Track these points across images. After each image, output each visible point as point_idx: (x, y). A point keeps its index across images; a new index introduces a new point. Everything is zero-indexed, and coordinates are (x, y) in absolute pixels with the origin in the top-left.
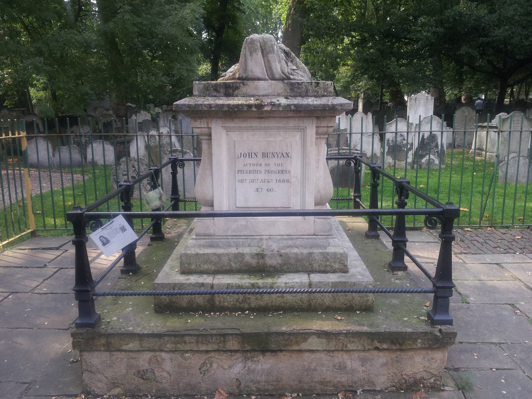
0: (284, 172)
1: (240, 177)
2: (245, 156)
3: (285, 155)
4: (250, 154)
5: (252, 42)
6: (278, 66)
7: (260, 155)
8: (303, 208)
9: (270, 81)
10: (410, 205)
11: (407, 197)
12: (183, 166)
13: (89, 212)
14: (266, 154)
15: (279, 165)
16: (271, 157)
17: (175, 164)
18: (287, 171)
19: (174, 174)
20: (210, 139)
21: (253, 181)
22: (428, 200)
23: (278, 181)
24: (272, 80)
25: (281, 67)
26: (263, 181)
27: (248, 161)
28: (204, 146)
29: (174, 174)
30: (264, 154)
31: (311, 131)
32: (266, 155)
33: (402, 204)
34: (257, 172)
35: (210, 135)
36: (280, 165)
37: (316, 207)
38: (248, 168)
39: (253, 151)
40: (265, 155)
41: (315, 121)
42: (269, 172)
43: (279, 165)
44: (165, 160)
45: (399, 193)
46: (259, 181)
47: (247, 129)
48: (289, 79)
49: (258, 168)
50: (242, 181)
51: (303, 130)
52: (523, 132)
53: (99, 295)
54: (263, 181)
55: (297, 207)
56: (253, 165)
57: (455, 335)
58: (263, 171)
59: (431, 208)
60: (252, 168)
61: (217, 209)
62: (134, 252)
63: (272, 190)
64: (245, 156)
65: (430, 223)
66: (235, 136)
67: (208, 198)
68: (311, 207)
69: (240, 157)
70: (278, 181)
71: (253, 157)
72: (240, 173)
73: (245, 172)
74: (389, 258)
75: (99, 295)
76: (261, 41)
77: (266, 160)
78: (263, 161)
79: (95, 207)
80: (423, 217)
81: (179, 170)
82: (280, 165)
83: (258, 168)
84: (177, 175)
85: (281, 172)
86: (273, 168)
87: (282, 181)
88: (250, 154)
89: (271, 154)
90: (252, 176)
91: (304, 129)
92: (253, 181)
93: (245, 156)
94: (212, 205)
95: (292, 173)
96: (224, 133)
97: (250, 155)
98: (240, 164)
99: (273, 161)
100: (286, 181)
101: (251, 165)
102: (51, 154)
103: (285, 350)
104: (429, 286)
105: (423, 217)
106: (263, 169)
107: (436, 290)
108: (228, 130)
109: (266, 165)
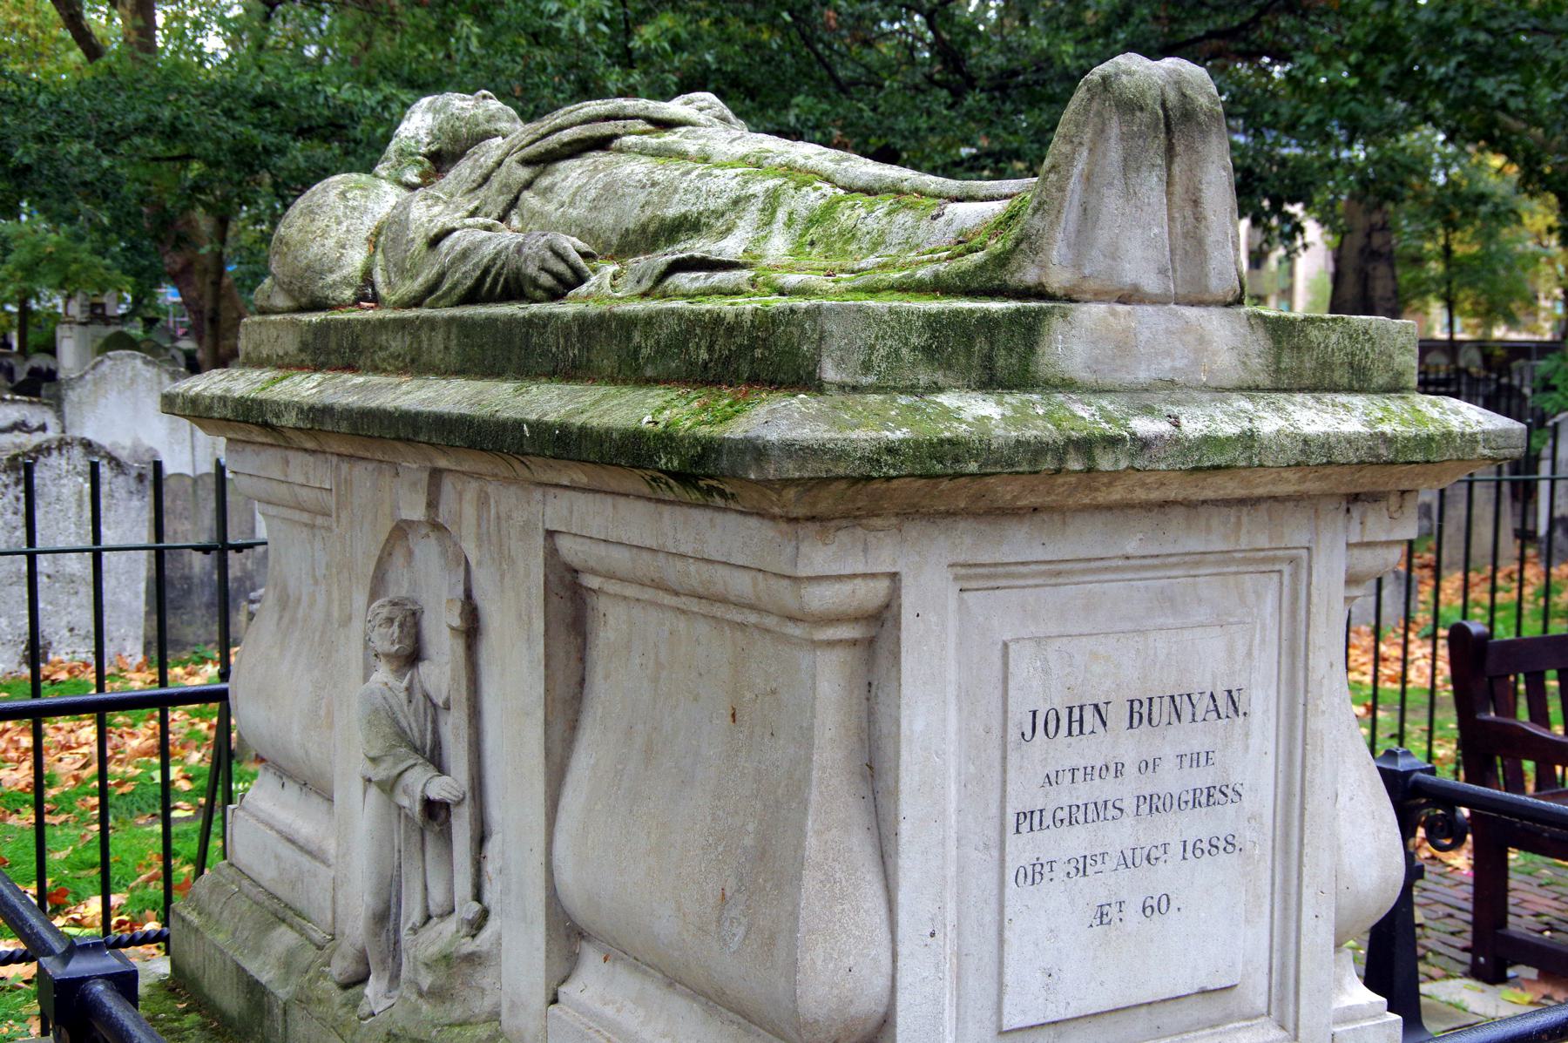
3: (1222, 701)
15: (1195, 760)
34: (1101, 810)
40: (1139, 713)
43: (1195, 760)
46: (1111, 863)
56: (1088, 772)
58: (1129, 804)
60: (1084, 792)
78: (1126, 745)
86: (1170, 780)
90: (1075, 841)
106: (1125, 790)
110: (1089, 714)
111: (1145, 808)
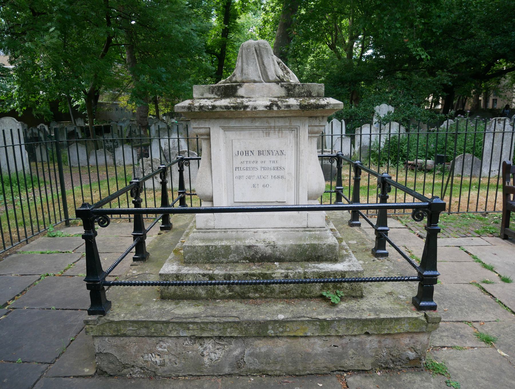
0: (279, 169)
1: (237, 173)
2: (242, 154)
4: (247, 152)
5: (248, 47)
6: (273, 69)
7: (256, 153)
8: (297, 203)
9: (265, 83)
10: (391, 199)
11: (389, 191)
12: (188, 164)
13: (98, 208)
14: (262, 152)
15: (274, 162)
16: (266, 154)
17: (182, 163)
18: (282, 168)
19: (181, 171)
20: (209, 139)
21: (250, 177)
22: (416, 196)
23: (273, 177)
24: (266, 82)
25: (276, 72)
26: (259, 177)
27: (245, 158)
28: (204, 145)
29: (181, 171)
30: (260, 152)
31: (304, 132)
32: (262, 152)
33: (384, 199)
35: (209, 135)
36: (275, 162)
37: (309, 201)
38: (245, 165)
39: (276, 171)
40: (260, 153)
41: (307, 121)
42: (264, 169)
43: (274, 162)
44: (174, 158)
45: (381, 186)
47: (243, 129)
48: (282, 81)
49: (254, 165)
50: (240, 177)
51: (297, 129)
52: (7, 147)
53: (110, 285)
54: (259, 177)
55: (291, 203)
57: (440, 319)
59: (418, 202)
60: (249, 165)
61: (217, 204)
62: (145, 242)
63: (267, 185)
64: (242, 153)
65: (418, 216)
66: (232, 135)
67: (208, 193)
68: (304, 202)
69: (237, 155)
70: (273, 177)
71: (249, 155)
72: (237, 170)
73: (242, 169)
74: (373, 245)
75: (110, 285)
76: (257, 46)
77: (262, 158)
79: (102, 203)
80: (410, 211)
81: (186, 168)
82: (275, 162)
83: (254, 165)
84: (184, 172)
85: (276, 169)
86: (267, 165)
87: (277, 177)
88: (247, 152)
89: (266, 151)
91: (297, 128)
92: (250, 177)
93: (242, 154)
94: (211, 200)
95: (286, 170)
96: (221, 131)
97: (247, 153)
98: (238, 161)
99: (266, 158)
100: (280, 177)
101: (248, 162)
102: (136, 162)
103: (282, 337)
104: (414, 273)
105: (410, 211)
106: (259, 165)
107: (421, 279)
108: (225, 129)
109: (262, 162)
110: (249, 152)
111: (263, 169)
